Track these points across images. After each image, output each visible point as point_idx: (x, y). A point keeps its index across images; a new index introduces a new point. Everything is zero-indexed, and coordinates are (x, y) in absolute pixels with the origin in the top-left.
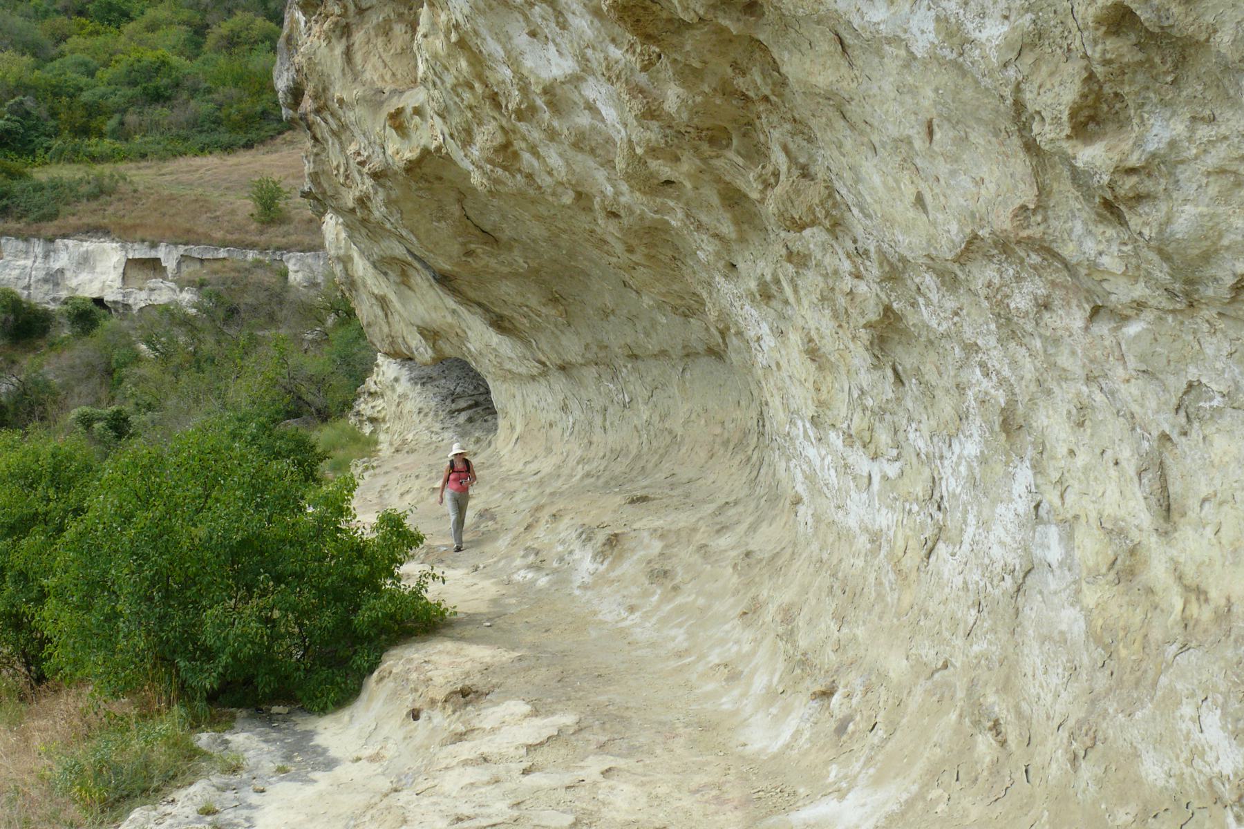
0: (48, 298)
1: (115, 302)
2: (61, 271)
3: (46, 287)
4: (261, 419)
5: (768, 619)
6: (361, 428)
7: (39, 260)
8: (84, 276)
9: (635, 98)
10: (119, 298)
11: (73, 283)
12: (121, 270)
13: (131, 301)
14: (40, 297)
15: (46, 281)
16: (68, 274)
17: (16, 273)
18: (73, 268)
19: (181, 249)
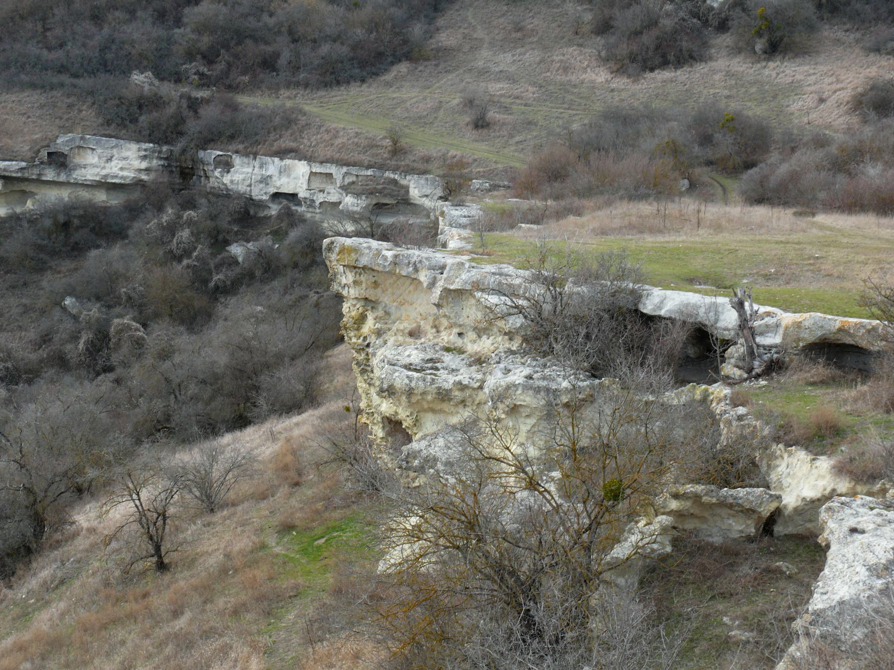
0: (262, 192)
1: (305, 198)
2: (270, 177)
3: (261, 186)
4: (351, 405)
5: (337, 143)
6: (705, 639)
7: (256, 169)
8: (284, 180)
9: (873, 462)
10: (307, 195)
11: (278, 184)
12: (307, 178)
13: (315, 198)
14: (259, 193)
15: (261, 182)
16: (274, 179)
17: (241, 177)
18: (277, 175)
19: (345, 169)
